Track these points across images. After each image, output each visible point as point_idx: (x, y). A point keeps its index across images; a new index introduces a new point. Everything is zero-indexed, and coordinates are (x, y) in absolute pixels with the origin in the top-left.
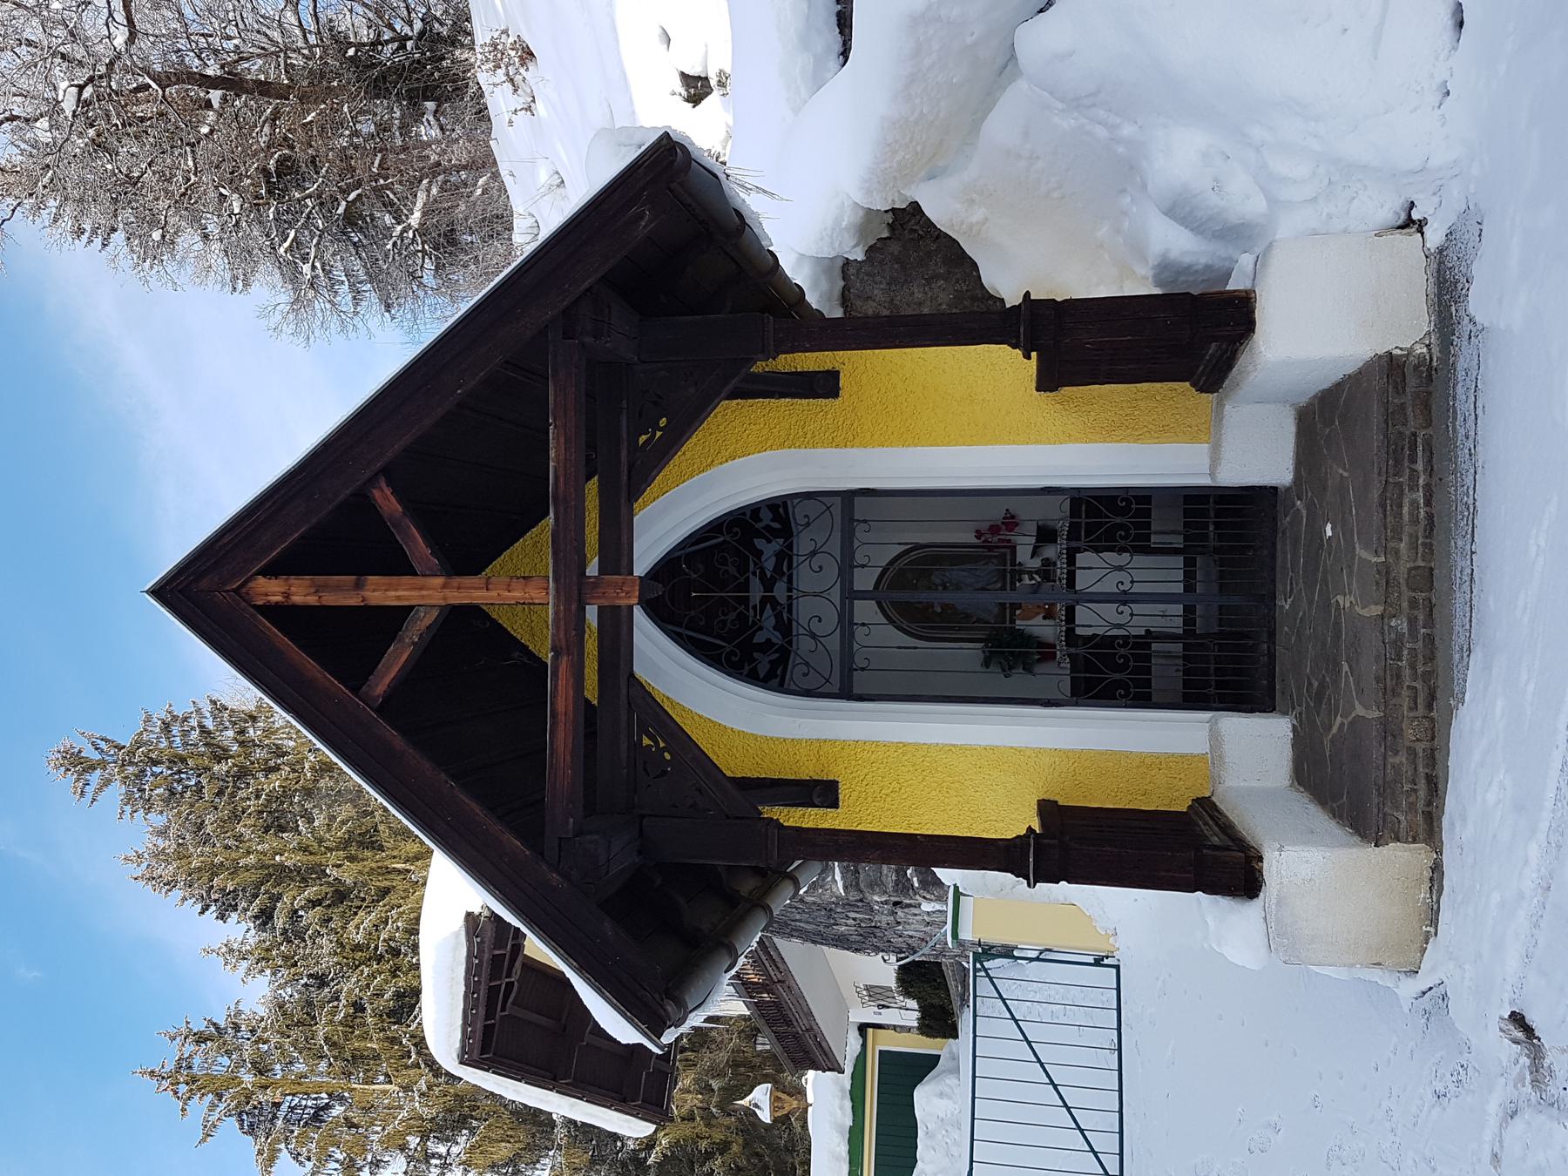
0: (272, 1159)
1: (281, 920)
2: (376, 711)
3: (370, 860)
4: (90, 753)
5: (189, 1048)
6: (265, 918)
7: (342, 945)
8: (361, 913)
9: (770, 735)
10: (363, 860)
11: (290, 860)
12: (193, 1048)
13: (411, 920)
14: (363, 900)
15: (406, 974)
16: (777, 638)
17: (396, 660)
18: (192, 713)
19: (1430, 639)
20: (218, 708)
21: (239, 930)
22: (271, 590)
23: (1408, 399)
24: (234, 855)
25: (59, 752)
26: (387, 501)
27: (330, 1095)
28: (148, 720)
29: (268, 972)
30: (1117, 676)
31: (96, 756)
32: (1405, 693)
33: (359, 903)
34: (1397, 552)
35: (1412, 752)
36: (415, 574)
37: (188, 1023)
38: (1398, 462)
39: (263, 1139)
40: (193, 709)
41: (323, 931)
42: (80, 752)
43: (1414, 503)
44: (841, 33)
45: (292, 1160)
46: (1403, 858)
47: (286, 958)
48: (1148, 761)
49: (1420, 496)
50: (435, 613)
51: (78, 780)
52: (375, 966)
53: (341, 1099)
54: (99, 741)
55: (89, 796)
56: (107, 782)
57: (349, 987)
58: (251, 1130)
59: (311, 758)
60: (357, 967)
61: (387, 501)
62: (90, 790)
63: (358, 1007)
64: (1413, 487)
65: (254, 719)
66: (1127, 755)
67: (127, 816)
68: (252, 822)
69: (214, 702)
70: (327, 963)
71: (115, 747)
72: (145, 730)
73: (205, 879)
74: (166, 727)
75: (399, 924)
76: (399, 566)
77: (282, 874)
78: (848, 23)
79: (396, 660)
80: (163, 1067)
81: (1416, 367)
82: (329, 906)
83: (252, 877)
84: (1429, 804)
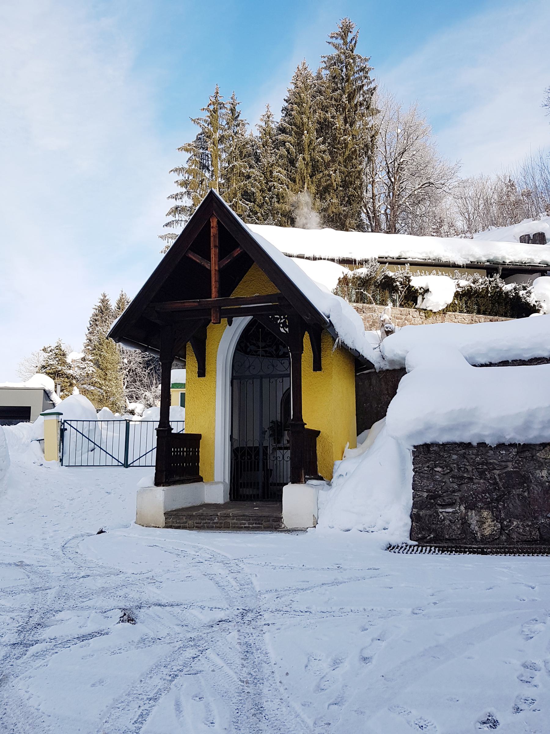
0: (187, 150)
1: (281, 138)
2: (185, 255)
3: (306, 173)
4: (350, 36)
5: (228, 106)
6: (282, 130)
7: (272, 165)
8: (285, 172)
9: (217, 356)
10: (307, 169)
11: (305, 138)
12: (229, 108)
13: (283, 194)
14: (291, 172)
15: (261, 195)
16: (281, 353)
17: (196, 258)
18: (369, 80)
19: (213, 527)
20: (372, 91)
21: (278, 117)
22: (214, 223)
23: (271, 522)
24: (307, 112)
25: (350, 23)
26: (237, 252)
27: (213, 171)
28: (366, 60)
29: (261, 135)
30: (239, 457)
31: (349, 40)
32: (200, 521)
33: (289, 170)
34: (234, 519)
35: (186, 523)
36: (219, 261)
37: (239, 103)
38: (255, 520)
39: (194, 145)
40: (371, 80)
41: (277, 157)
42: (350, 32)
43: (245, 524)
44: (500, 363)
45: (188, 158)
46: (162, 519)
47: (266, 141)
48: (212, 465)
49: (247, 525)
50: (209, 268)
51: (337, 34)
52: (264, 182)
53: (212, 176)
54: (355, 40)
55: (330, 40)
56: (336, 47)
57: (255, 172)
58: (198, 139)
59: (349, 139)
60: (263, 174)
61: (237, 252)
62: (334, 40)
63: (249, 177)
64: (249, 524)
65: (368, 108)
66: (214, 459)
67: (323, 59)
68: (322, 116)
69: (374, 89)
70: (264, 161)
71: (352, 48)
72: (362, 60)
73: (297, 101)
74: (362, 70)
75: (281, 189)
76: (221, 256)
77: (300, 134)
78: (504, 365)
79: (196, 258)
80: (220, 97)
81: (279, 525)
82: (288, 157)
83: (298, 122)
84: (174, 527)
